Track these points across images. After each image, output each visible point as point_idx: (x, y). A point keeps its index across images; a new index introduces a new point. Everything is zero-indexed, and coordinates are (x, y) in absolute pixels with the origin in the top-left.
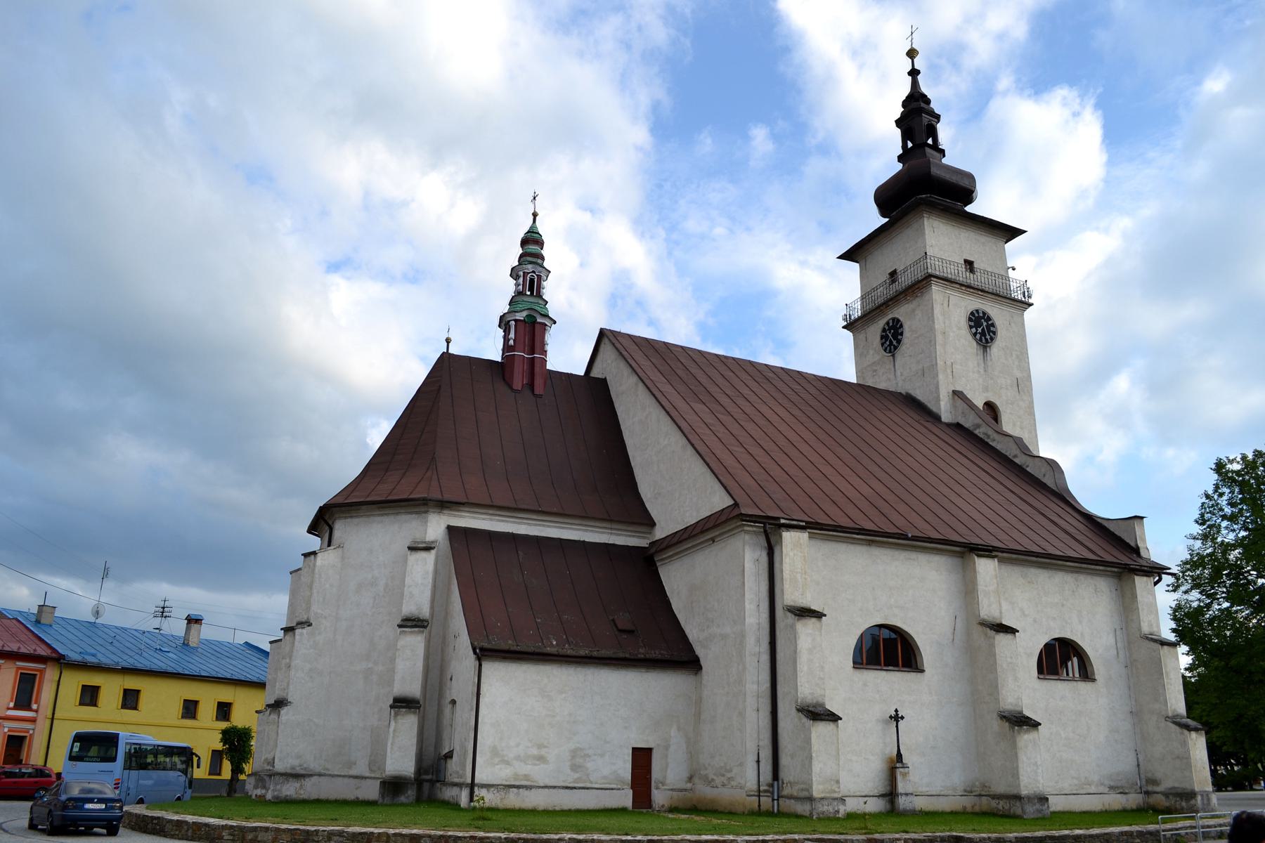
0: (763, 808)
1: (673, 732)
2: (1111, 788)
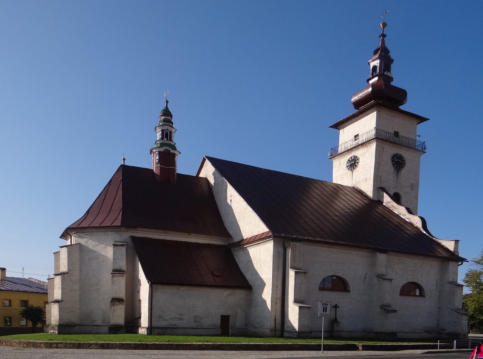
0: (285, 333)
2: (425, 331)
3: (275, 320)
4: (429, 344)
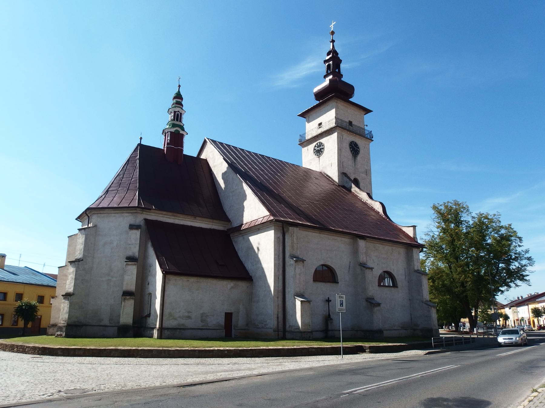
0: (287, 334)
1: (241, 306)
3: (278, 318)
4: (395, 344)
